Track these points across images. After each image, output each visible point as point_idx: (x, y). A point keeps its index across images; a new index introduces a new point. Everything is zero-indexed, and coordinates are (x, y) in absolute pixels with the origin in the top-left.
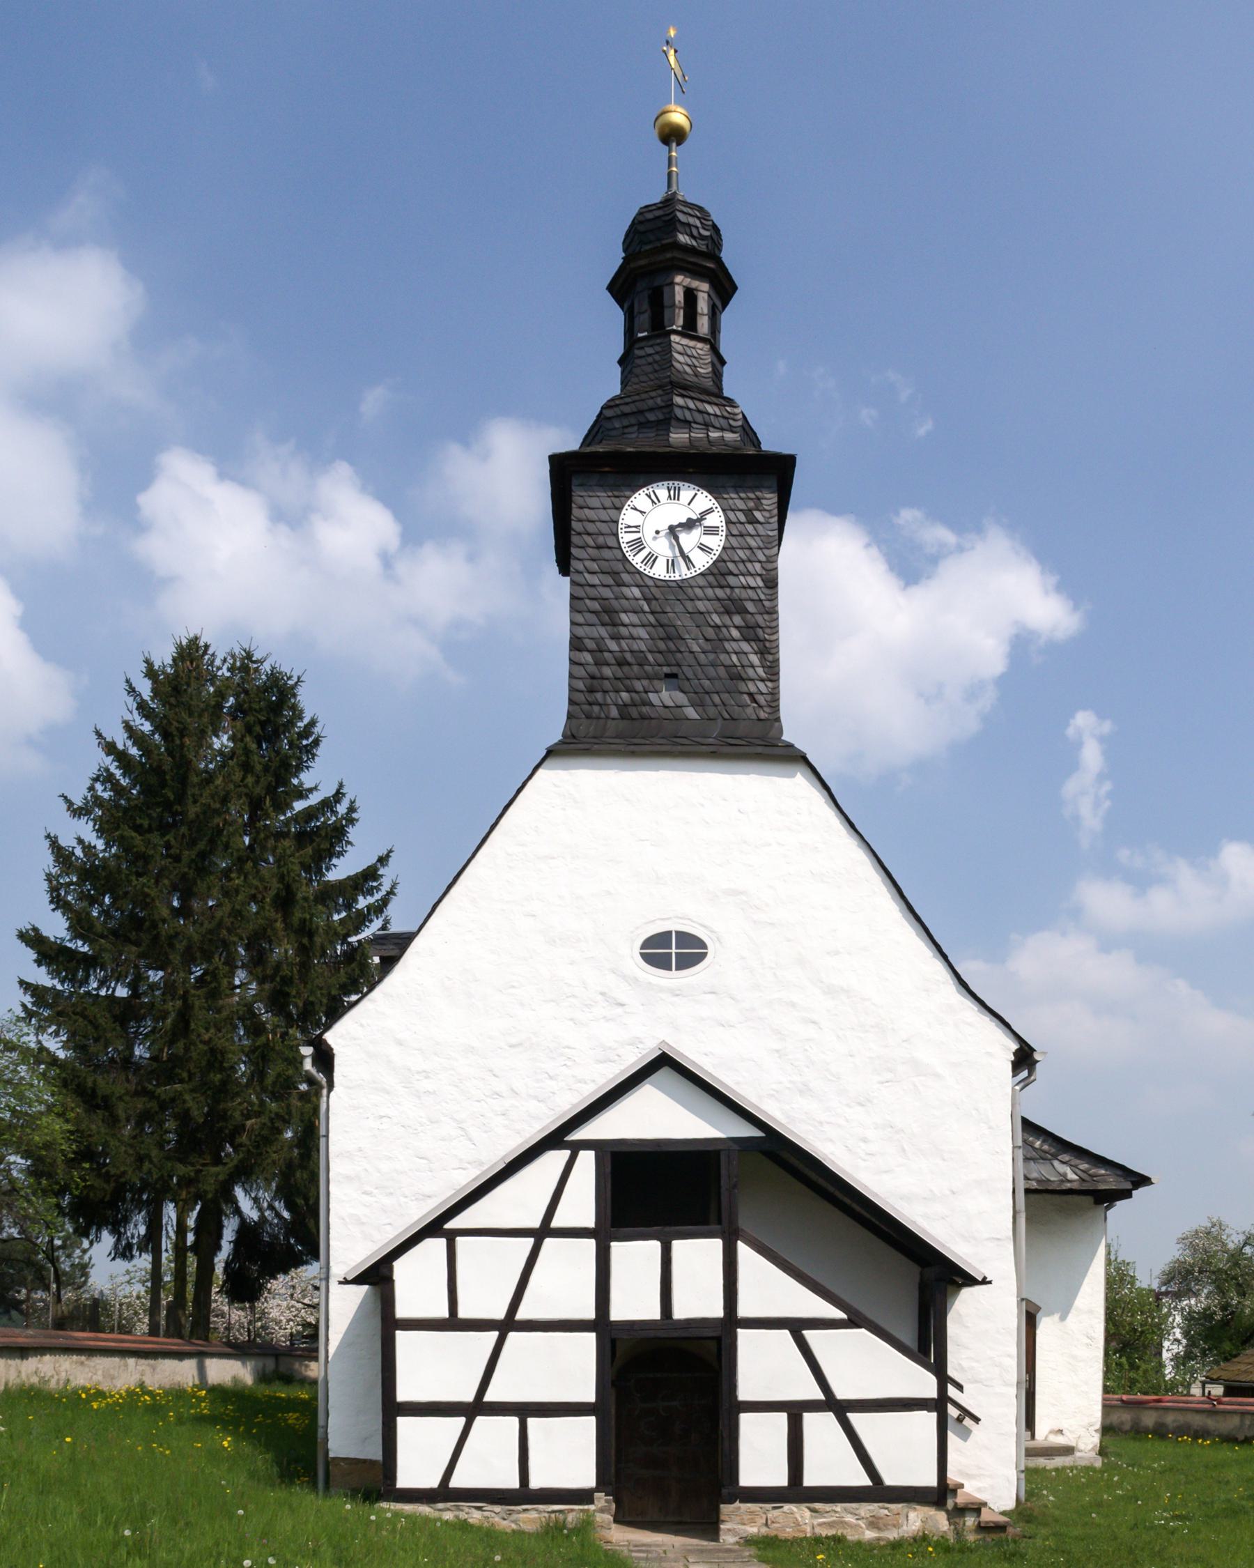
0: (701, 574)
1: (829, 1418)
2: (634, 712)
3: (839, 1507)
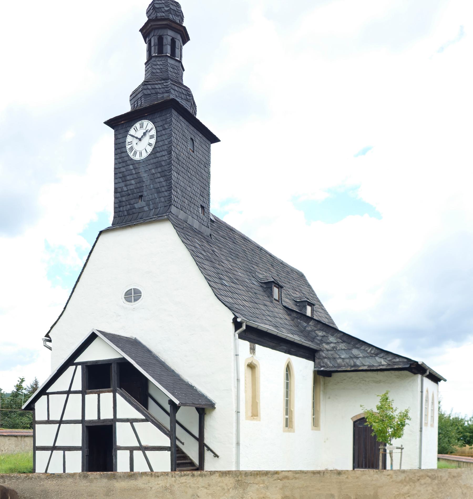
1: (140, 452)
2: (131, 212)
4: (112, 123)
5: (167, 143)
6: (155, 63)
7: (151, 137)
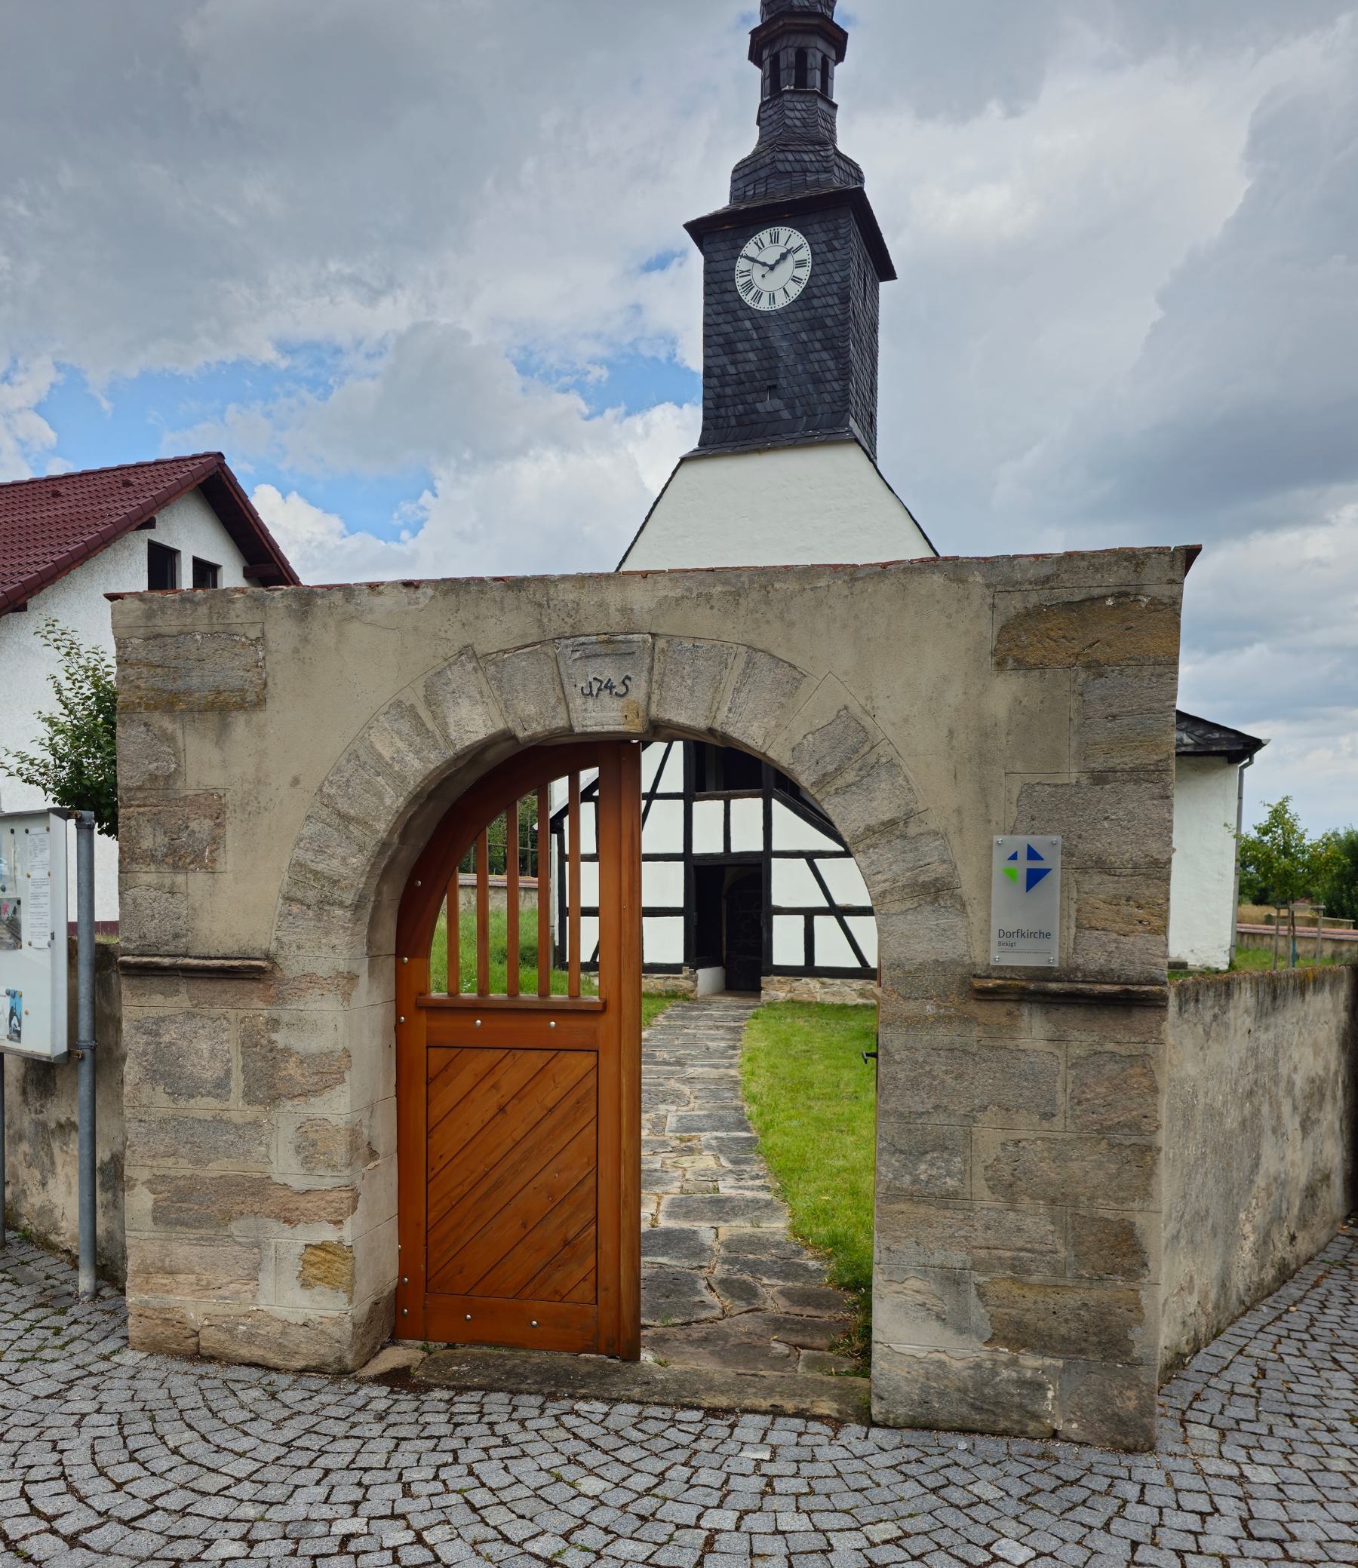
1: (832, 920)
3: (838, 981)
4: (701, 230)
5: (837, 279)
6: (791, 105)
7: (800, 264)
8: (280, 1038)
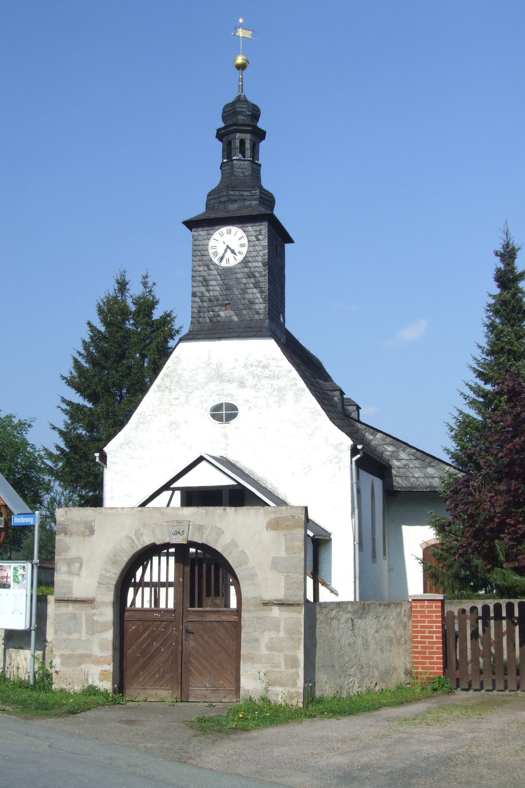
0: (240, 263)
2: (215, 320)
8: (96, 618)
